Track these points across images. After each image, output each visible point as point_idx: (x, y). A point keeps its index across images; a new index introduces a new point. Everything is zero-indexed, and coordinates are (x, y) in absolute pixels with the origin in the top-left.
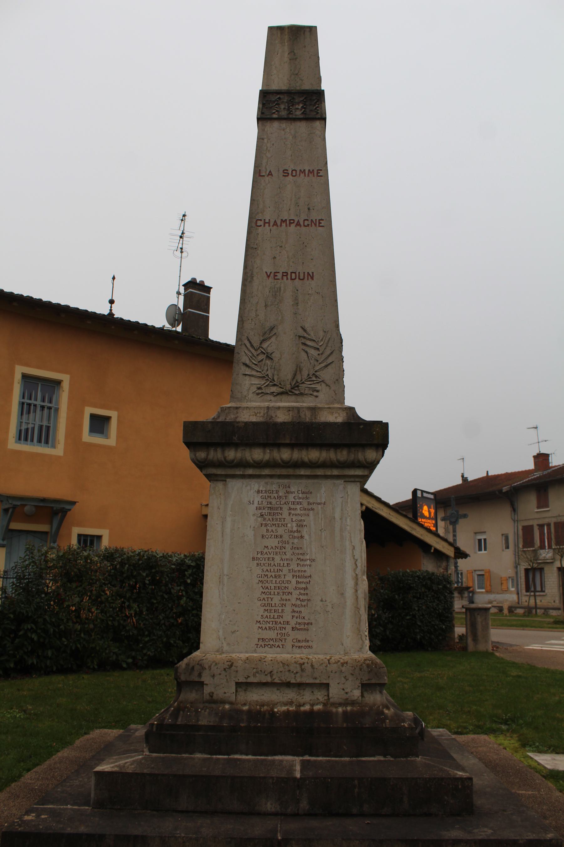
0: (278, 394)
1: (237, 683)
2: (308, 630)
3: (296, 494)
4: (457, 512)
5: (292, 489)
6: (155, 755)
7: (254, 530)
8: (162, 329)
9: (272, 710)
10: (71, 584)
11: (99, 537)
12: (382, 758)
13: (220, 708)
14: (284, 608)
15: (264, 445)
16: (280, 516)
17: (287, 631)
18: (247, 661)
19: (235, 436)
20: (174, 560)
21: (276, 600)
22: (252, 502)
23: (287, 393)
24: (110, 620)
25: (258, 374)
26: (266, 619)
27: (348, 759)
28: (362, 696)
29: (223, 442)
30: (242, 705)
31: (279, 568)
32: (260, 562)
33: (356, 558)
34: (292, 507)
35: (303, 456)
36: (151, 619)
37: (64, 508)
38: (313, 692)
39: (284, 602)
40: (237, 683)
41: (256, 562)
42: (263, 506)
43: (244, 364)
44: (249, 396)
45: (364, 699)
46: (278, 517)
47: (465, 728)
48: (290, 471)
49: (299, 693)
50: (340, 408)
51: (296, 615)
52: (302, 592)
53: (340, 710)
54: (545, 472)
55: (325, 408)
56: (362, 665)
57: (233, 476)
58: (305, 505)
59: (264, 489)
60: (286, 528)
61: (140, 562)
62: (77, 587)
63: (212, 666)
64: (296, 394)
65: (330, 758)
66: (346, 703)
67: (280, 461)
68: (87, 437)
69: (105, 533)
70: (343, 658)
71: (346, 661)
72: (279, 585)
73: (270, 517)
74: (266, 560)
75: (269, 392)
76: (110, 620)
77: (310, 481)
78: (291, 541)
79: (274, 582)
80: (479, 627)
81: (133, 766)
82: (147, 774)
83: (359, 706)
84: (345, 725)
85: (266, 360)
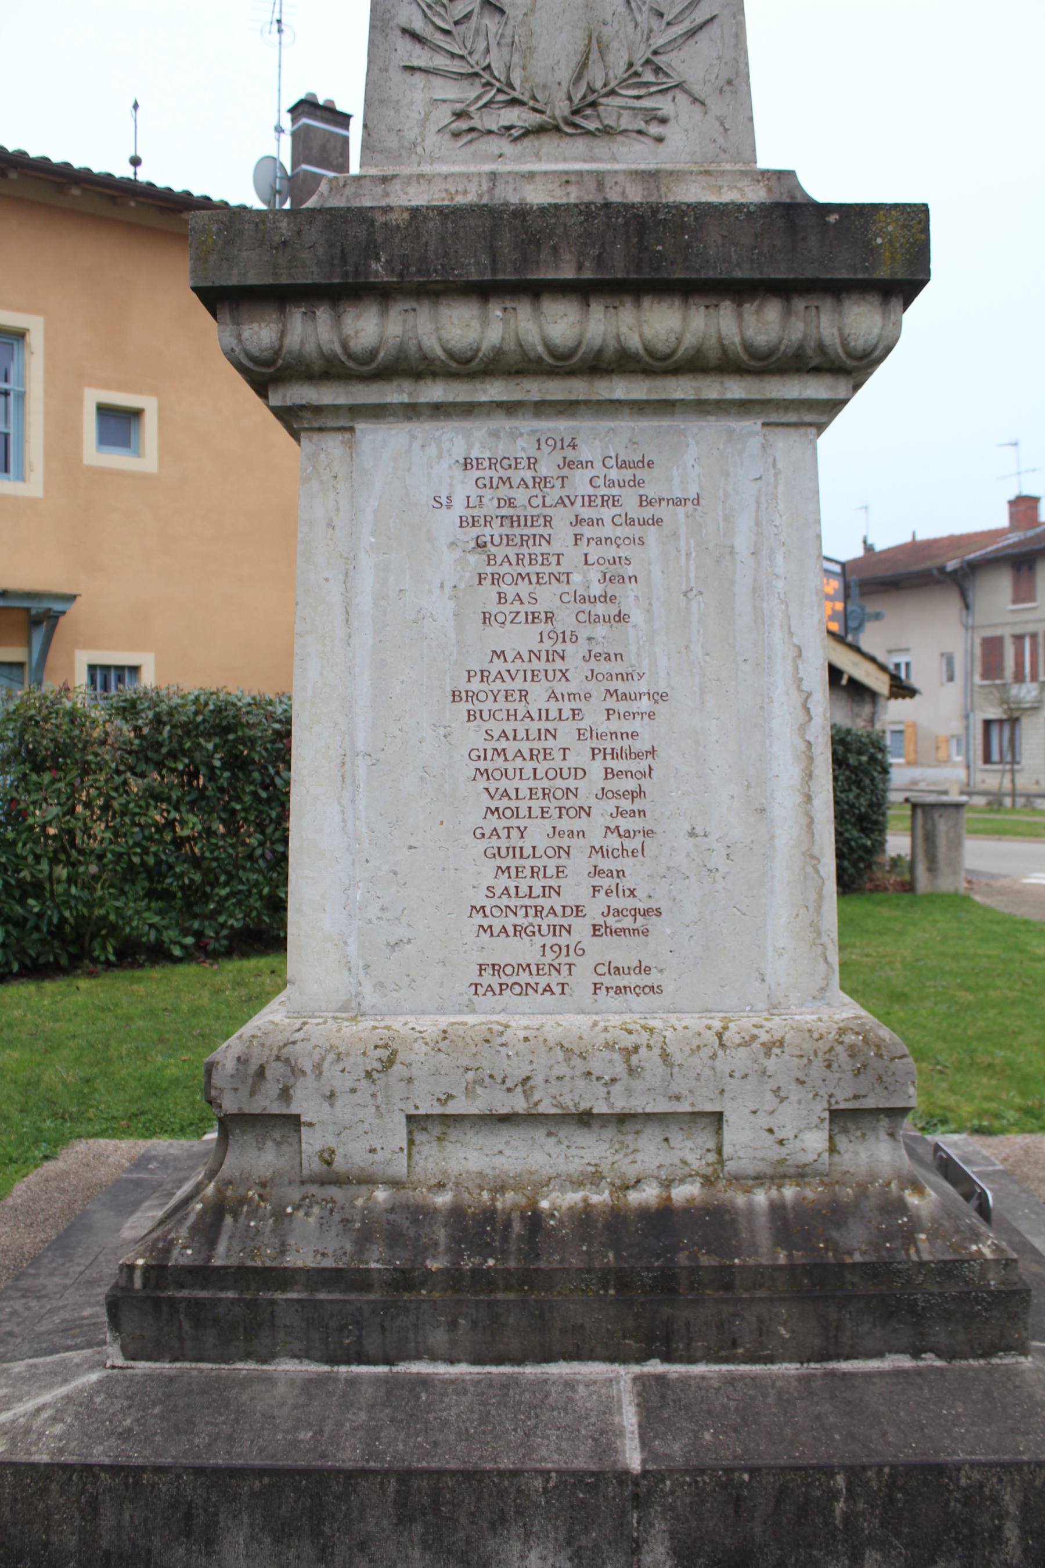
0: (527, 133)
1: (410, 1118)
2: (646, 933)
3: (598, 470)
4: (863, 608)
5: (585, 453)
6: (143, 1366)
7: (454, 597)
8: (243, 208)
9: (533, 1205)
10: (39, 776)
11: (135, 670)
12: (905, 1362)
13: (359, 1202)
14: (563, 861)
15: (483, 291)
16: (545, 548)
17: (575, 937)
18: (443, 1045)
19: (378, 259)
20: (279, 711)
21: (538, 833)
22: (444, 500)
23: (557, 129)
24: (135, 854)
25: (457, 66)
26: (505, 901)
27: (791, 1368)
28: (833, 1150)
29: (336, 281)
30: (430, 1189)
31: (544, 725)
32: (481, 706)
33: (805, 686)
34: (586, 513)
35: (624, 329)
36: (232, 846)
37: (50, 610)
38: (666, 1140)
39: (565, 842)
40: (410, 1118)
41: (464, 706)
42: (484, 511)
43: (405, 31)
44: (427, 143)
45: (836, 1158)
46: (537, 550)
47: (998, 1116)
48: (578, 388)
49: (622, 1143)
50: (744, 174)
51: (606, 882)
52: (626, 804)
53: (761, 1198)
54: (1031, 533)
55: (691, 173)
56: (831, 1049)
57: (378, 412)
58: (634, 511)
59: (487, 454)
60: (566, 588)
61: (200, 718)
62: (54, 781)
63: (326, 1065)
64: (588, 133)
65: (731, 1367)
66: (776, 1176)
67: (540, 349)
68: (93, 454)
69: (147, 661)
70: (768, 1025)
71: (777, 1036)
72: (545, 783)
73: (511, 552)
74: (501, 697)
75: (494, 127)
76: (135, 854)
77: (647, 424)
78: (583, 632)
79: (528, 773)
80: (942, 842)
81: (58, 1429)
82: (103, 1467)
83: (822, 1183)
84: (782, 1258)
85: (481, 14)
